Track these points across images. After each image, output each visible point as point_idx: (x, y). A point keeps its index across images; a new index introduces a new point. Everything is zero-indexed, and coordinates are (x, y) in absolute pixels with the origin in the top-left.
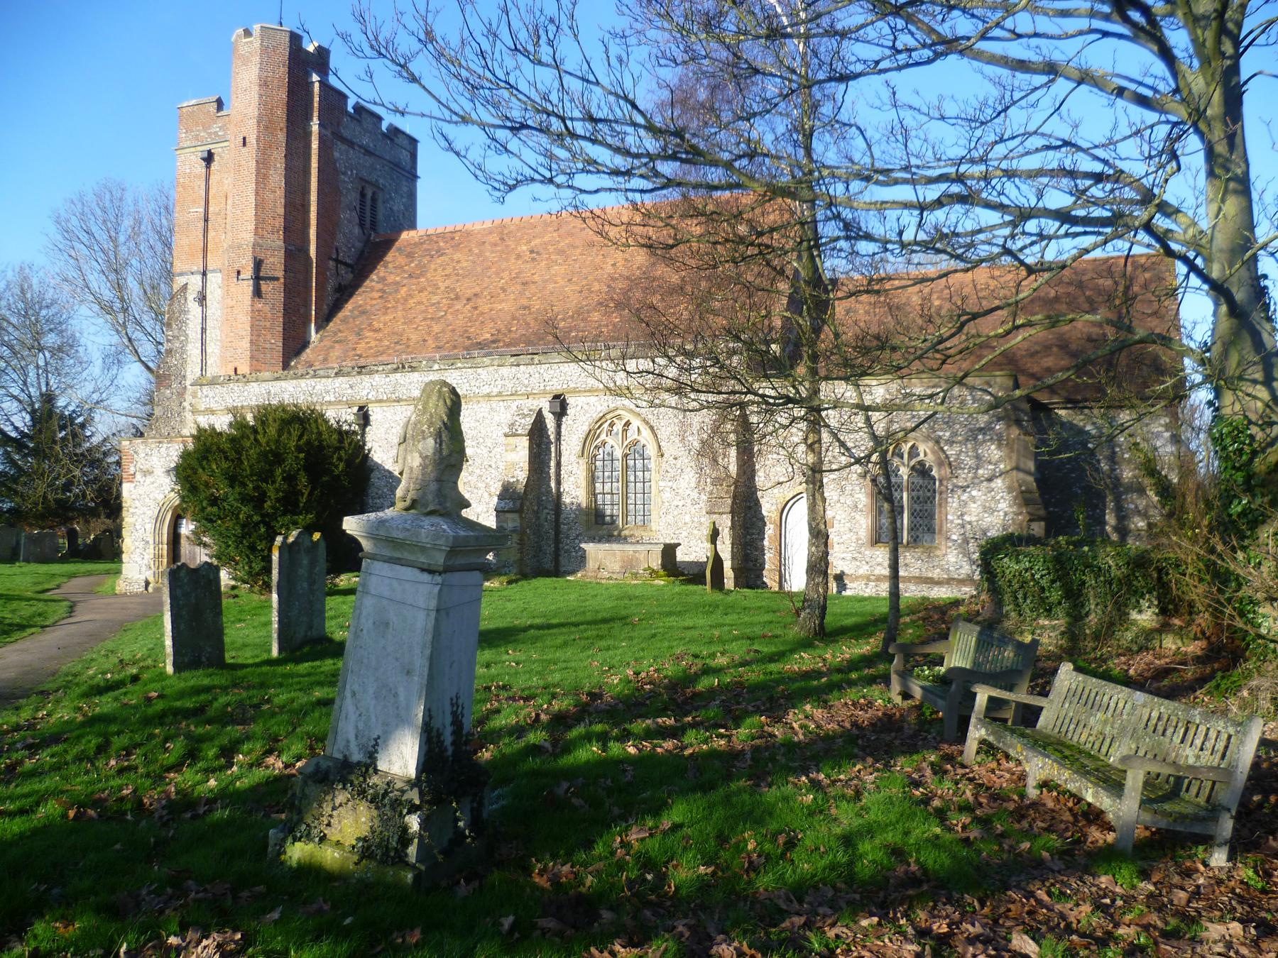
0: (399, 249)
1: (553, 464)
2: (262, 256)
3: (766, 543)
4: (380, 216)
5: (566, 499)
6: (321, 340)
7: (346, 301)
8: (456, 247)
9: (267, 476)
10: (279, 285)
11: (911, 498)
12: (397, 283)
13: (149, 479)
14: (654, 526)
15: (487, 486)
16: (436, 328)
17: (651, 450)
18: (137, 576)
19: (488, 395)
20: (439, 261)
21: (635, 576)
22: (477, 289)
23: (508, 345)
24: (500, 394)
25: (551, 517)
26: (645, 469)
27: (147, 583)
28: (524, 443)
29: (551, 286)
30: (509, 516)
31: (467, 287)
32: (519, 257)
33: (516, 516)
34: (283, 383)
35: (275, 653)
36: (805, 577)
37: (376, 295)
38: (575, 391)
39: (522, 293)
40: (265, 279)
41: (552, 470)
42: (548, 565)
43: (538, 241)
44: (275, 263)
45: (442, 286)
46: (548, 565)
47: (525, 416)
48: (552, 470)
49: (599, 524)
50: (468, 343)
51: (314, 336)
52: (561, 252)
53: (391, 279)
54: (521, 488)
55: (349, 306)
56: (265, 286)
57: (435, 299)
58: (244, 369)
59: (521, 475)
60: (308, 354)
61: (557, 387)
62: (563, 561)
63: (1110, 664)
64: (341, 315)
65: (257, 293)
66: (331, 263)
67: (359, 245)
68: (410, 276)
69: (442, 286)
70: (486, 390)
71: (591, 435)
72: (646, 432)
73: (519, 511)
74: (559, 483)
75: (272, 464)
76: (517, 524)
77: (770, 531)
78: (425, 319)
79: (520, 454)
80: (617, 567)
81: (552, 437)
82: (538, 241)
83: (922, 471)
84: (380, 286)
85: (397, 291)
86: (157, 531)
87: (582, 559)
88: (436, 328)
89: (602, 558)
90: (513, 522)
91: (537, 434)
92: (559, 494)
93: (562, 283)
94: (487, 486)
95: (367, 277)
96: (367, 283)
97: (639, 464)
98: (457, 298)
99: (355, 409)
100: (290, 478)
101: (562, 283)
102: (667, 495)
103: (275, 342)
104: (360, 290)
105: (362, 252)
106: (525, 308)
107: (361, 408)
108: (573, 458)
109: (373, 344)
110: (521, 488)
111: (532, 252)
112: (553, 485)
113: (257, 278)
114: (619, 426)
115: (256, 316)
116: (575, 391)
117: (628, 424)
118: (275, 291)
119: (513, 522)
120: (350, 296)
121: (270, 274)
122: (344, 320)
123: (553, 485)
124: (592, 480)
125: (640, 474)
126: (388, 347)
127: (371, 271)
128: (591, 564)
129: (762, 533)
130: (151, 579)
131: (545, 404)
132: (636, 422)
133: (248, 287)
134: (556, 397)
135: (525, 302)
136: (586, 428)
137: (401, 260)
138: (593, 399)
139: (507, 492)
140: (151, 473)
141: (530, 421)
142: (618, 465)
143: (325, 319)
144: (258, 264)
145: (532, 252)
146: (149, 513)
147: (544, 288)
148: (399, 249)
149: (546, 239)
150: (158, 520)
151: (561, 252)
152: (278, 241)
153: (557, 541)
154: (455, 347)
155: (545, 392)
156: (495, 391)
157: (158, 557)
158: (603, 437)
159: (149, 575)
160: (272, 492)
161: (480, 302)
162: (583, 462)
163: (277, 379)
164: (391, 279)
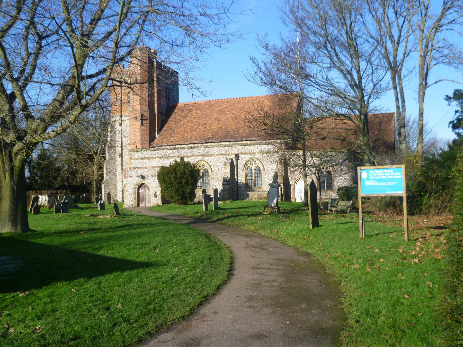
0: (178, 109)
1: (236, 172)
2: (143, 113)
3: (291, 191)
4: (171, 98)
5: (239, 181)
6: (159, 137)
7: (165, 125)
8: (197, 108)
9: (182, 178)
10: (148, 121)
11: (327, 179)
12: (180, 119)
13: (132, 178)
14: (263, 187)
15: (218, 178)
16: (195, 133)
17: (262, 168)
18: (129, 204)
19: (218, 155)
20: (192, 113)
21: (261, 199)
22: (205, 122)
23: (217, 139)
24: (221, 154)
25: (236, 186)
26: (260, 173)
27: (132, 205)
28: (229, 167)
29: (227, 121)
30: (226, 186)
31: (202, 121)
32: (216, 112)
33: (228, 186)
34: (158, 151)
35: (214, 209)
36: (304, 195)
37: (174, 123)
38: (241, 153)
39: (219, 123)
40: (144, 120)
41: (236, 174)
42: (235, 198)
43: (221, 107)
44: (147, 114)
45: (194, 121)
46: (235, 198)
47: (228, 160)
48: (236, 174)
49: (248, 187)
50: (205, 138)
51: (157, 136)
52: (229, 111)
53: (177, 118)
54: (228, 179)
55: (166, 126)
56: (144, 122)
57: (193, 125)
58: (139, 146)
59: (228, 175)
60: (156, 141)
61: (236, 152)
62: (239, 197)
63: (24, 6)
64: (163, 129)
65: (142, 124)
66: (160, 114)
67: (166, 107)
68: (184, 117)
69: (194, 121)
70: (217, 153)
71: (246, 164)
72: (260, 164)
73: (229, 184)
74: (237, 177)
75: (183, 175)
76: (228, 187)
77: (292, 188)
78: (190, 131)
79: (228, 170)
80: (256, 197)
81: (235, 165)
82: (221, 107)
83: (329, 172)
84: (174, 120)
85: (180, 122)
86: (134, 192)
87: (248, 195)
88: (195, 133)
89: (253, 196)
90: (227, 187)
91: (232, 164)
92: (238, 180)
93: (230, 120)
94: (218, 178)
95: (170, 117)
96: (170, 119)
97: (258, 171)
98: (199, 124)
99: (180, 158)
100: (187, 178)
101: (230, 120)
102: (266, 180)
103: (147, 138)
104: (169, 121)
105: (167, 109)
106: (220, 128)
107: (181, 158)
108: (241, 171)
109: (176, 138)
110: (228, 179)
111: (220, 111)
112: (236, 177)
113: (142, 120)
114: (253, 162)
115: (142, 131)
116: (241, 153)
117: (255, 162)
118: (146, 123)
119: (227, 187)
120: (166, 123)
121: (146, 118)
122: (165, 131)
123: (236, 177)
124: (246, 176)
125: (259, 174)
126: (181, 139)
127: (171, 116)
128: (250, 197)
129: (290, 188)
130: (133, 204)
131: (233, 157)
132: (257, 162)
133: (139, 122)
134: (236, 155)
135: (220, 126)
136: (244, 163)
137: (180, 112)
138: (246, 155)
139: (225, 180)
140: (132, 177)
141: (230, 161)
142: (253, 172)
143: (160, 130)
144: (142, 116)
145: (220, 111)
146: (132, 187)
147: (225, 122)
148: (178, 109)
149: (224, 107)
150: (135, 189)
151: (229, 111)
152: (146, 108)
153: (237, 192)
154: (201, 139)
155: (233, 154)
156: (219, 153)
157: (134, 198)
158: (249, 165)
159: (133, 203)
160: (184, 181)
161: (206, 126)
162: (244, 172)
163: (156, 150)
164: (177, 118)
